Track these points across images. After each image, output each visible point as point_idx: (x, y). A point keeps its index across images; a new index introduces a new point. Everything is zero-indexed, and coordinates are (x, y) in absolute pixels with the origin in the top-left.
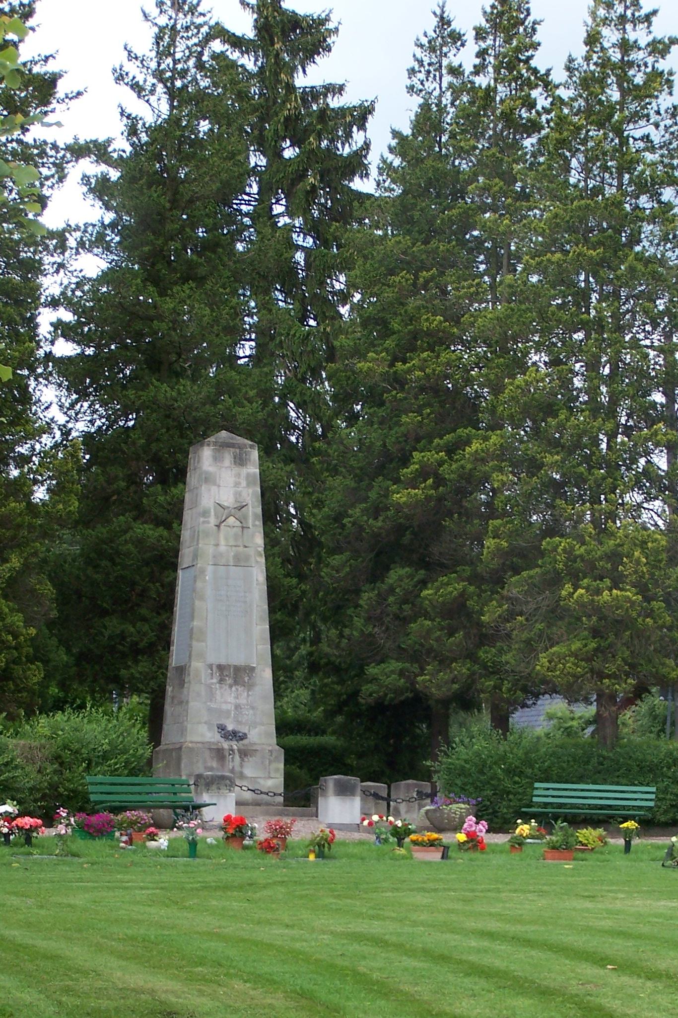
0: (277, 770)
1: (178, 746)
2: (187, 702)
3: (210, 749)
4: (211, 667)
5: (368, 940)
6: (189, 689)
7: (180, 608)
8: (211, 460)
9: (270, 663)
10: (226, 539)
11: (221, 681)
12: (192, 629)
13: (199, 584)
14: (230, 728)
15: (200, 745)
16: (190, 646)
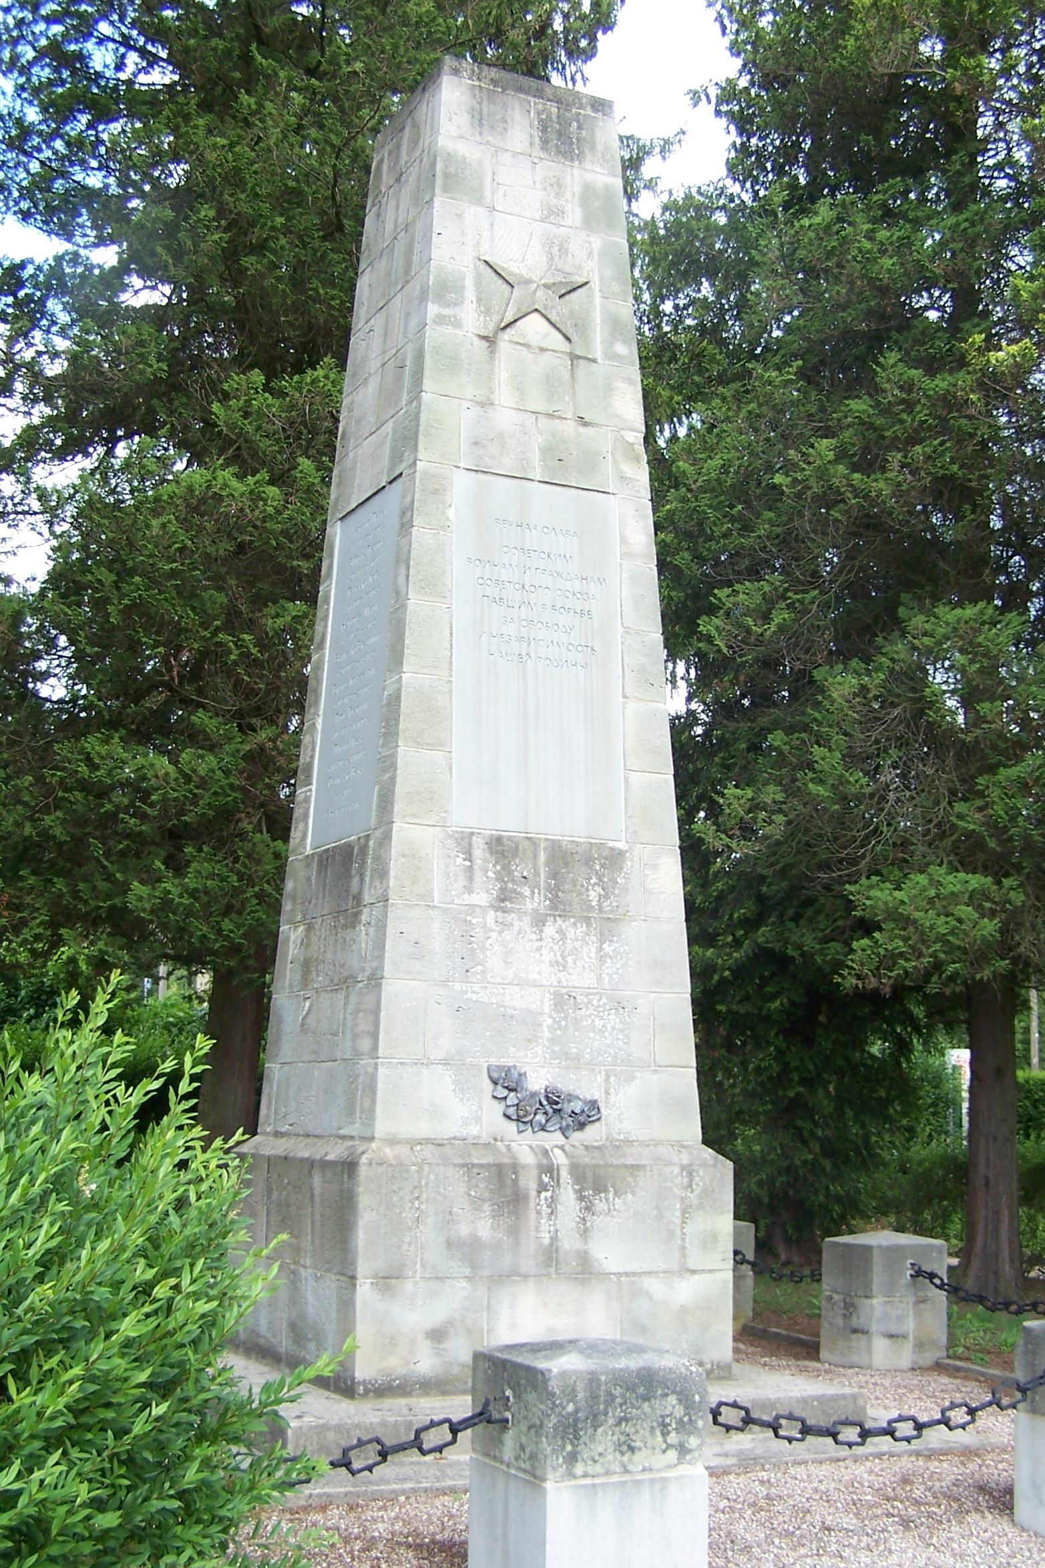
1: (335, 1152)
2: (375, 980)
3: (468, 1167)
4: (465, 843)
6: (382, 928)
7: (336, 651)
8: (464, 119)
10: (520, 389)
11: (504, 899)
12: (395, 699)
13: (421, 535)
14: (537, 1082)
16: (388, 765)
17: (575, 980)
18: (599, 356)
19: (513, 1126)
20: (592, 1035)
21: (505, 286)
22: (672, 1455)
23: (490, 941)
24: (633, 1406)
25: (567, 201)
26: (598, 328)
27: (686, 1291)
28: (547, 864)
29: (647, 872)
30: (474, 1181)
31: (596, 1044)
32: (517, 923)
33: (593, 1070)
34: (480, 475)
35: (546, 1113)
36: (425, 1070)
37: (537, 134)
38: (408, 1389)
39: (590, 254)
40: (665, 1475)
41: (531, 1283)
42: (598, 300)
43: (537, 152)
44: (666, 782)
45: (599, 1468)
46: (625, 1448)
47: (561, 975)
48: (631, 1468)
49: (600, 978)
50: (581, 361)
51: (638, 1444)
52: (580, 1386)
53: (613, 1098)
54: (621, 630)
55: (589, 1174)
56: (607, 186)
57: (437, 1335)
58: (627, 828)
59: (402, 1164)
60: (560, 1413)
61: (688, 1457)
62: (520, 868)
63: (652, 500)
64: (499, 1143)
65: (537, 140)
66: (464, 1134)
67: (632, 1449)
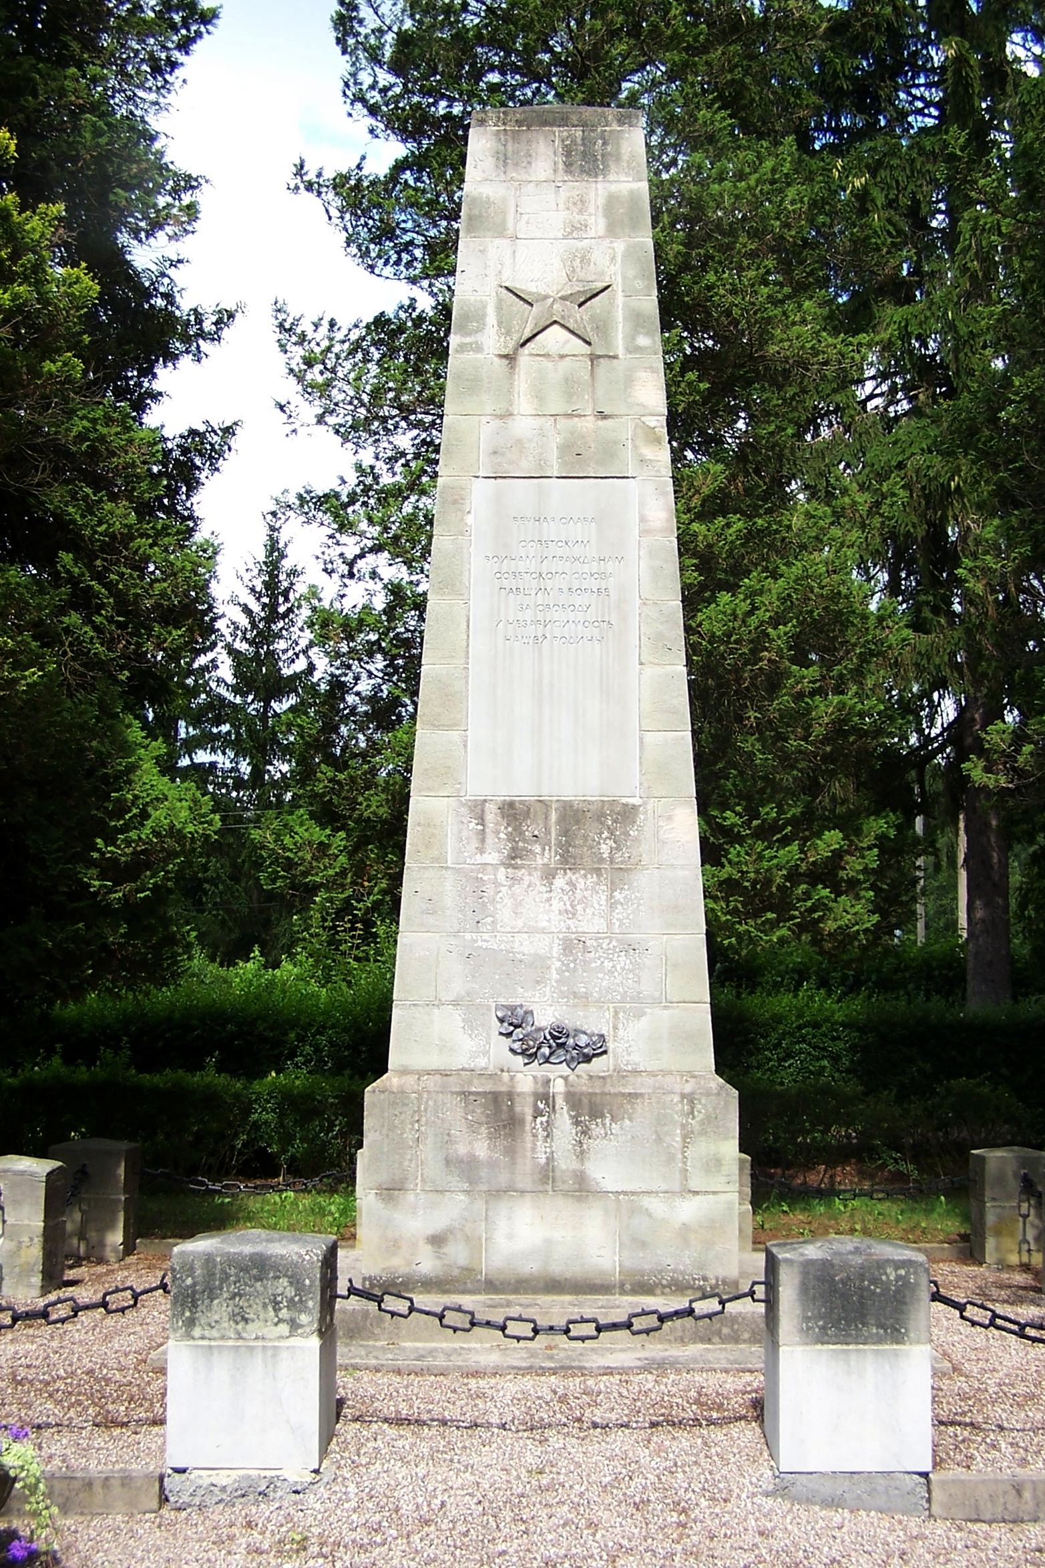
0: (715, 1164)
3: (465, 1094)
4: (478, 810)
5: (386, 1420)
8: (490, 162)
9: (692, 790)
10: (539, 396)
11: (515, 857)
14: (545, 1017)
15: (431, 1082)
17: (585, 926)
18: (620, 351)
19: (520, 1060)
20: (601, 975)
21: (526, 306)
22: (284, 1329)
23: (500, 895)
24: (246, 1284)
25: (590, 215)
26: (620, 326)
27: (688, 1210)
28: (558, 823)
29: (661, 823)
30: (470, 1107)
31: (605, 983)
32: (527, 878)
33: (601, 1007)
34: (499, 480)
35: (550, 1047)
36: (436, 1011)
37: (560, 160)
38: (411, 1286)
39: (613, 259)
40: (276, 1344)
41: (528, 1197)
42: (620, 299)
43: (561, 176)
44: (683, 738)
45: (215, 1333)
46: (239, 1318)
47: (569, 922)
48: (244, 1335)
49: (610, 924)
50: (602, 360)
51: (251, 1316)
52: (197, 1264)
53: (621, 1033)
54: (638, 602)
55: (585, 1101)
56: (632, 192)
57: (437, 1241)
58: (641, 784)
59: (403, 1092)
60: (180, 1286)
61: (300, 1331)
62: (530, 829)
63: (673, 477)
64: (505, 1074)
65: (561, 166)
66: (472, 1066)
67: (246, 1320)
